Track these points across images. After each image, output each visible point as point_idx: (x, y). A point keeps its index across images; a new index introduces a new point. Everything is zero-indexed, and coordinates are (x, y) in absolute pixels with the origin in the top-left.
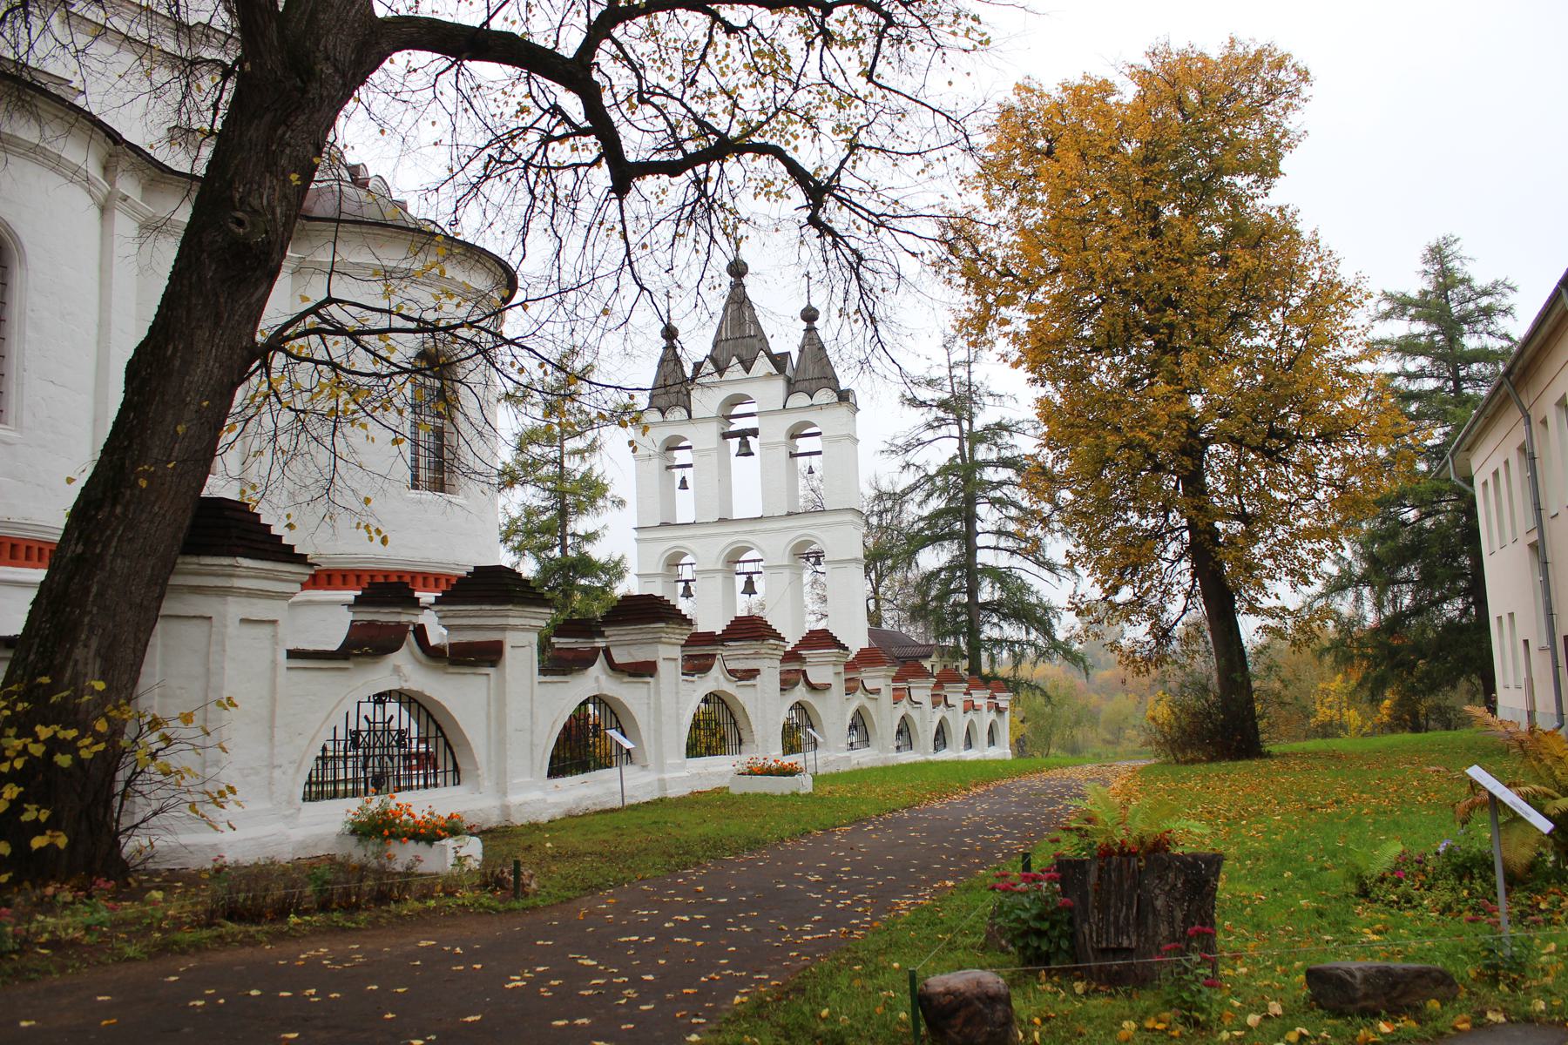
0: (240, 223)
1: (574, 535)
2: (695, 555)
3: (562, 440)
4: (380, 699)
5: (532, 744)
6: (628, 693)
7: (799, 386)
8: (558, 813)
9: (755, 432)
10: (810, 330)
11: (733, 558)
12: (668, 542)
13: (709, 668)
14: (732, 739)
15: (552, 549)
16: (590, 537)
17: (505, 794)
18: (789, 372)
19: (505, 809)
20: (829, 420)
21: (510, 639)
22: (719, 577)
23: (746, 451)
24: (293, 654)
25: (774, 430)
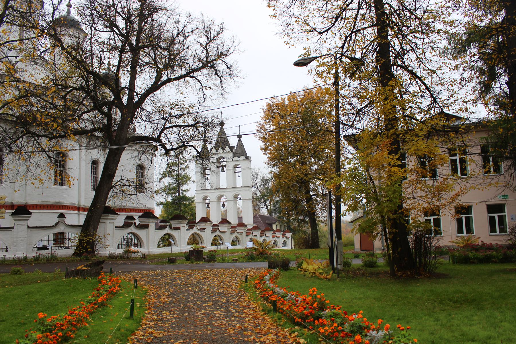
0: (110, 171)
1: (182, 190)
2: (210, 197)
3: (179, 165)
4: (129, 234)
5: (154, 242)
6: (174, 233)
7: (237, 155)
8: (158, 253)
9: (225, 166)
10: (240, 140)
11: (220, 198)
12: (204, 194)
13: (193, 228)
14: (200, 242)
15: (176, 193)
16: (186, 191)
17: (149, 249)
18: (234, 151)
19: (149, 252)
20: (243, 164)
21: (150, 224)
22: (216, 203)
23: (223, 171)
24: (116, 227)
25: (231, 165)
